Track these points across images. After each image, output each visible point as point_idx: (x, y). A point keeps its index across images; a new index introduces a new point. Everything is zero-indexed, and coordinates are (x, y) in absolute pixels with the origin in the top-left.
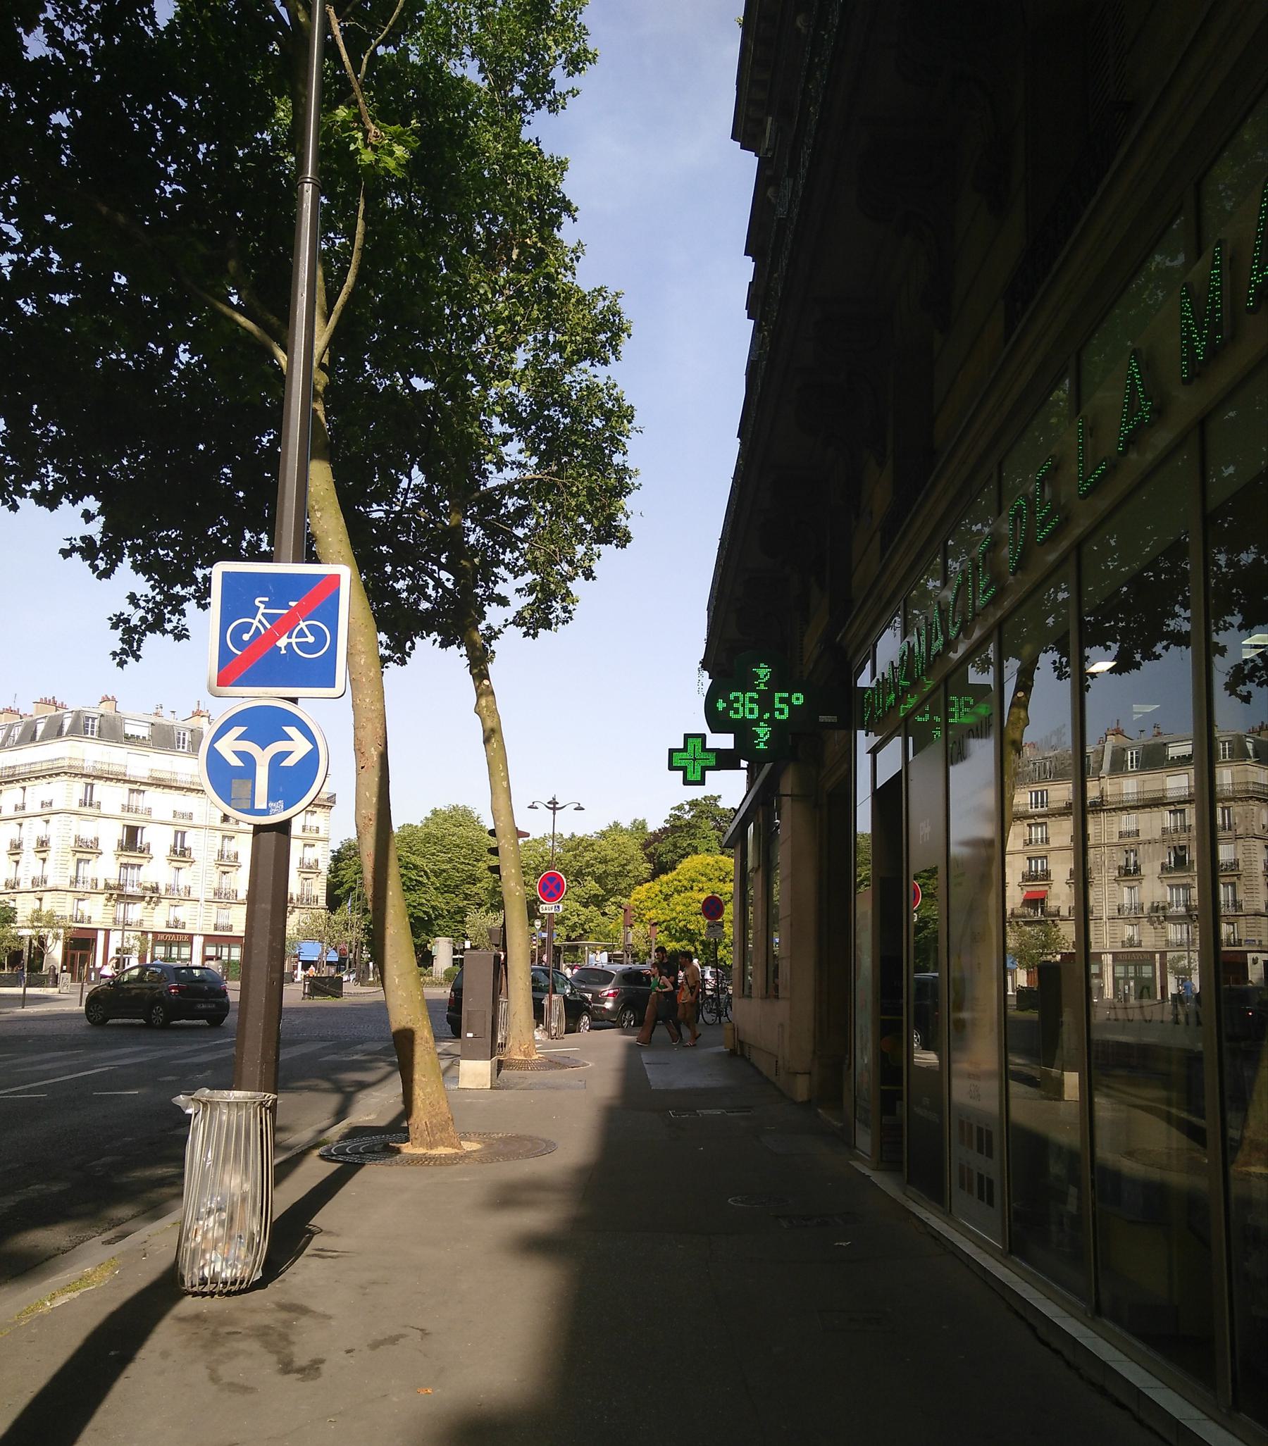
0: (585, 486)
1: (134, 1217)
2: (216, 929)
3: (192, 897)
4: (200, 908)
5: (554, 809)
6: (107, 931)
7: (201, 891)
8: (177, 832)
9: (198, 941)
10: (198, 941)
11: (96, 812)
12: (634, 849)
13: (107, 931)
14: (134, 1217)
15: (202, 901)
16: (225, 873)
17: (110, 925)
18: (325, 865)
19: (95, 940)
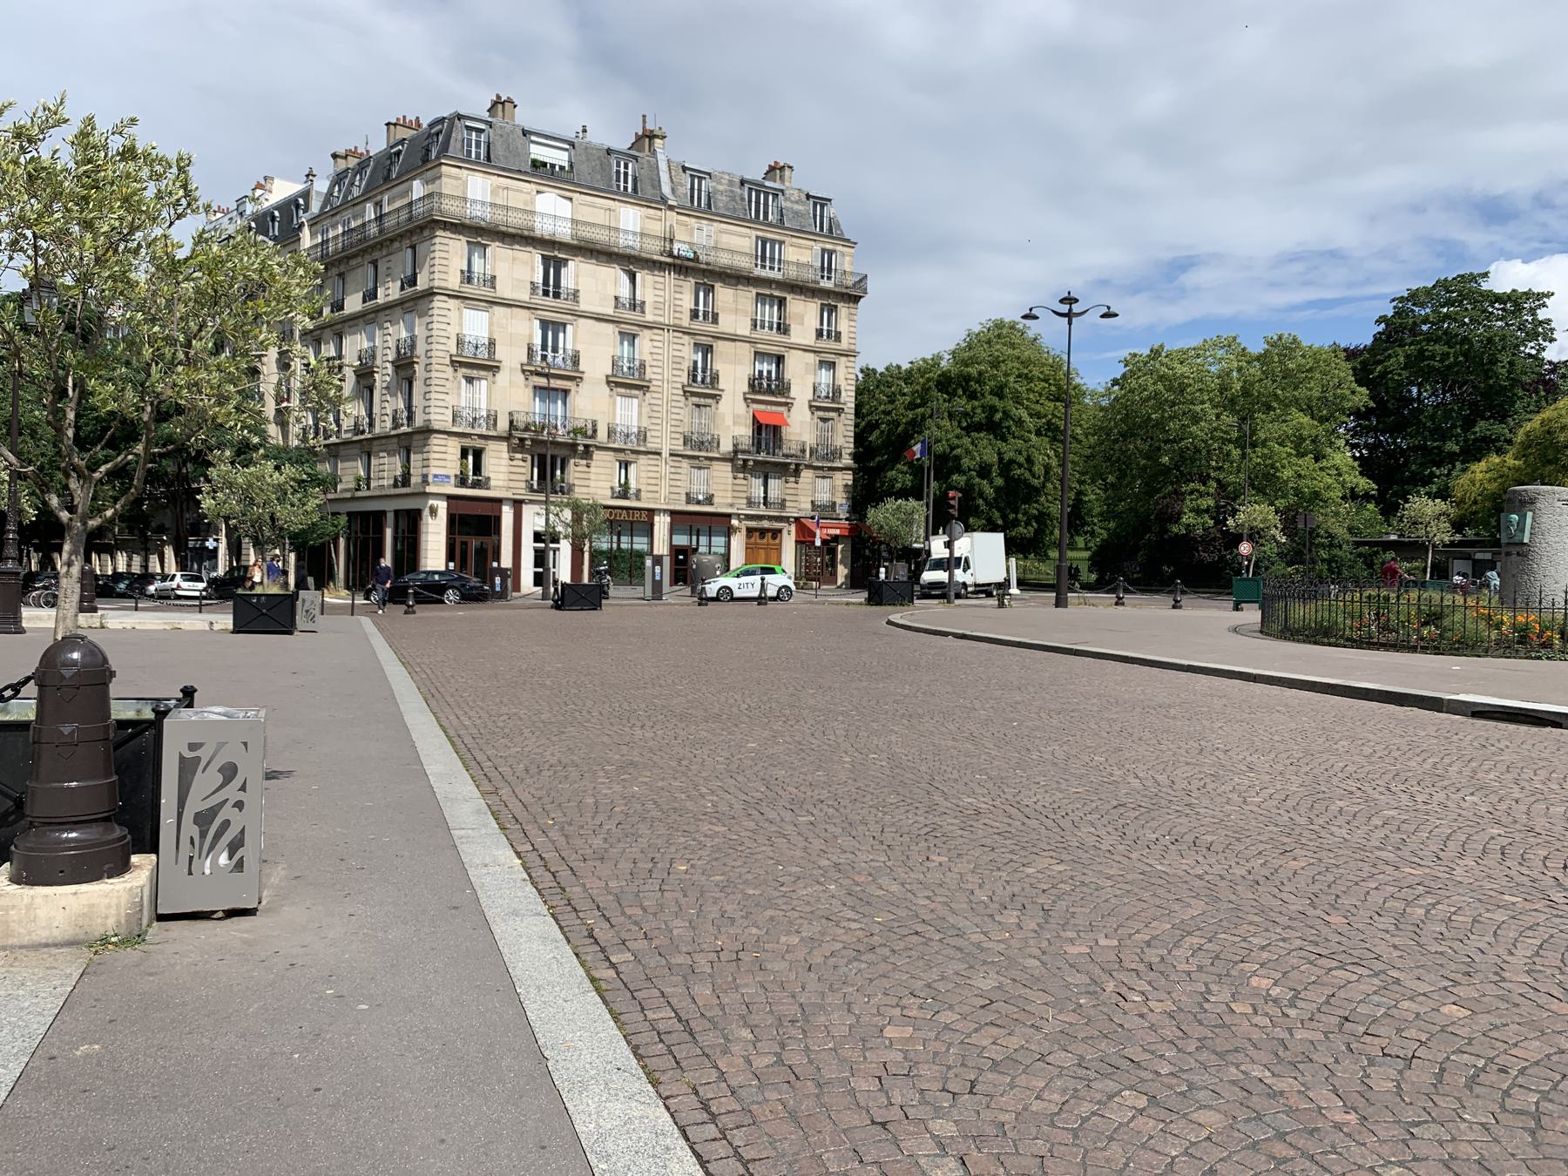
0: (332, 576)
1: (565, 403)
2: (688, 502)
3: (651, 446)
4: (664, 467)
5: (1069, 315)
6: (517, 504)
7: (665, 440)
8: (823, 251)
9: (662, 524)
10: (662, 524)
11: (485, 292)
12: (1345, 371)
13: (517, 504)
14: (565, 403)
15: (665, 454)
16: (698, 406)
17: (521, 492)
18: (848, 399)
19: (498, 519)
